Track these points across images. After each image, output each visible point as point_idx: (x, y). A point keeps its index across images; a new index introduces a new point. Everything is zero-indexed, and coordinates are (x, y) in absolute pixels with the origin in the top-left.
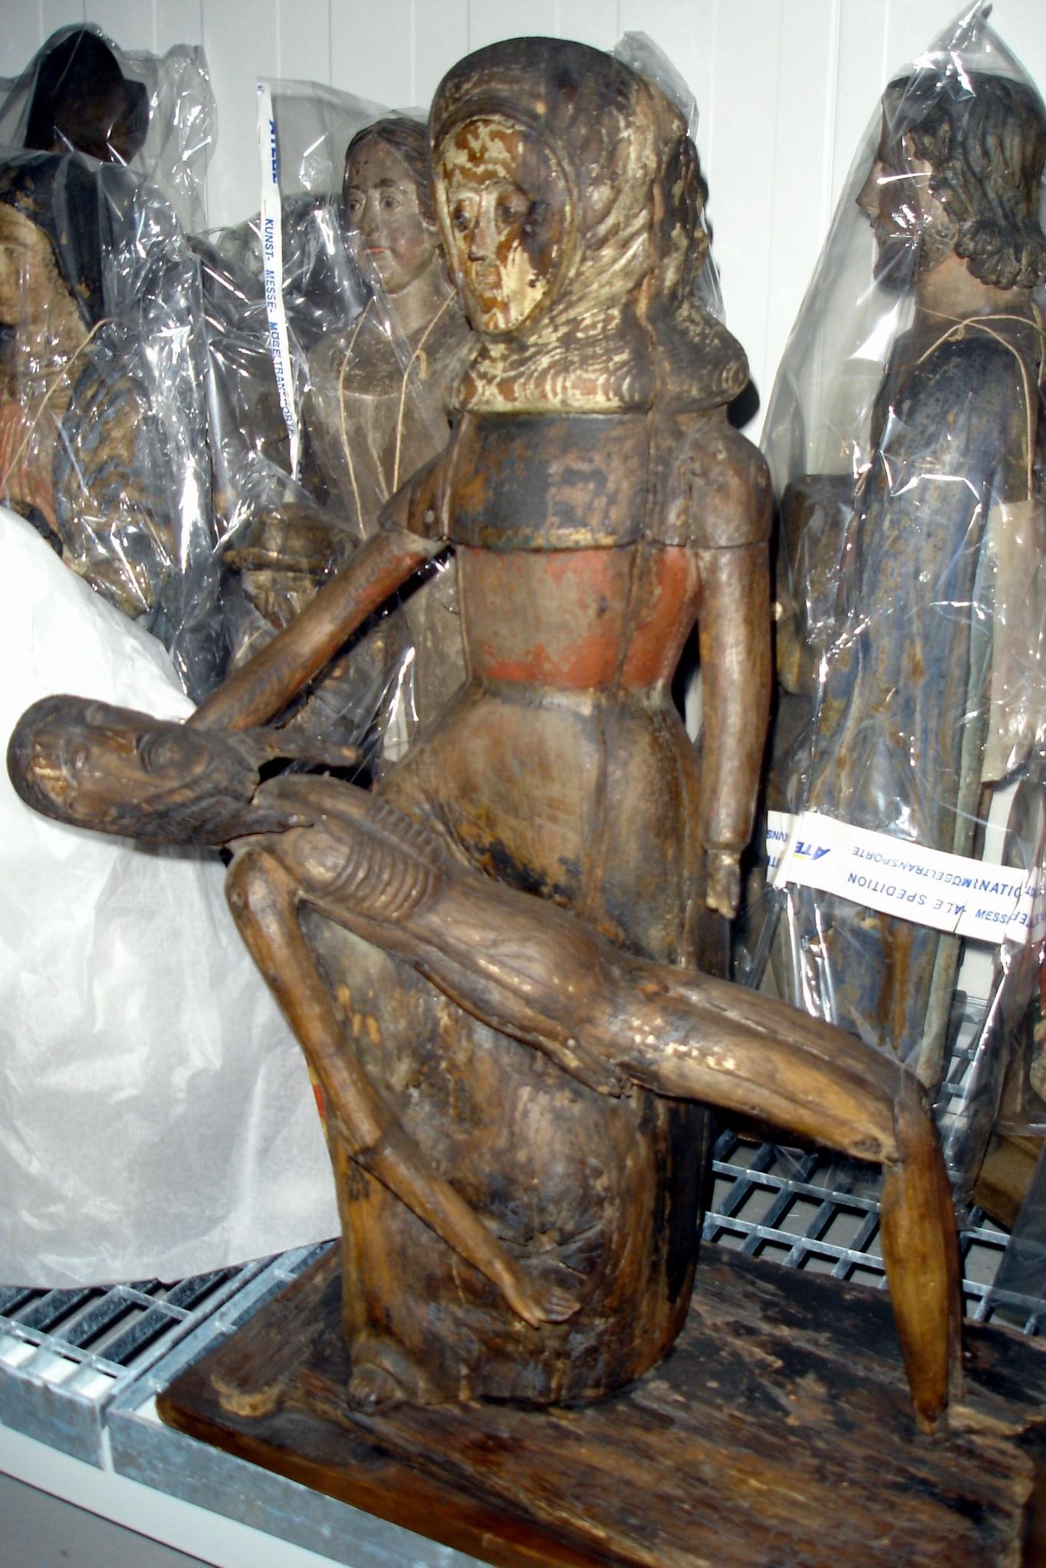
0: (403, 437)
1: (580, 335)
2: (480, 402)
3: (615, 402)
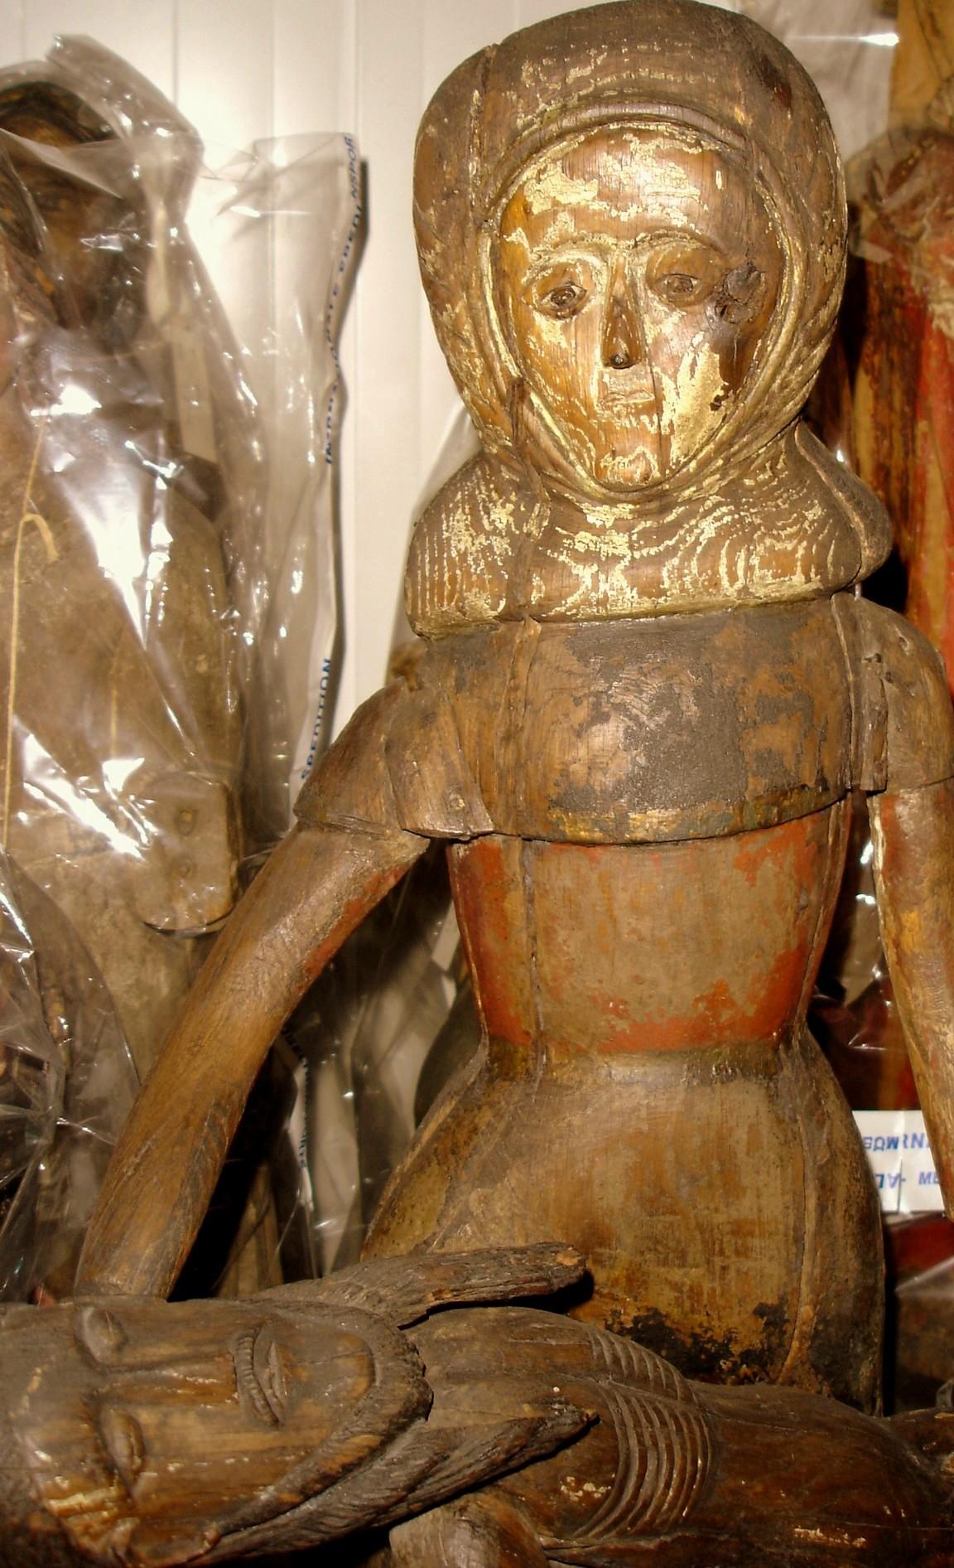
0: (20, 657)
1: (748, 482)
2: (586, 602)
3: (816, 584)
